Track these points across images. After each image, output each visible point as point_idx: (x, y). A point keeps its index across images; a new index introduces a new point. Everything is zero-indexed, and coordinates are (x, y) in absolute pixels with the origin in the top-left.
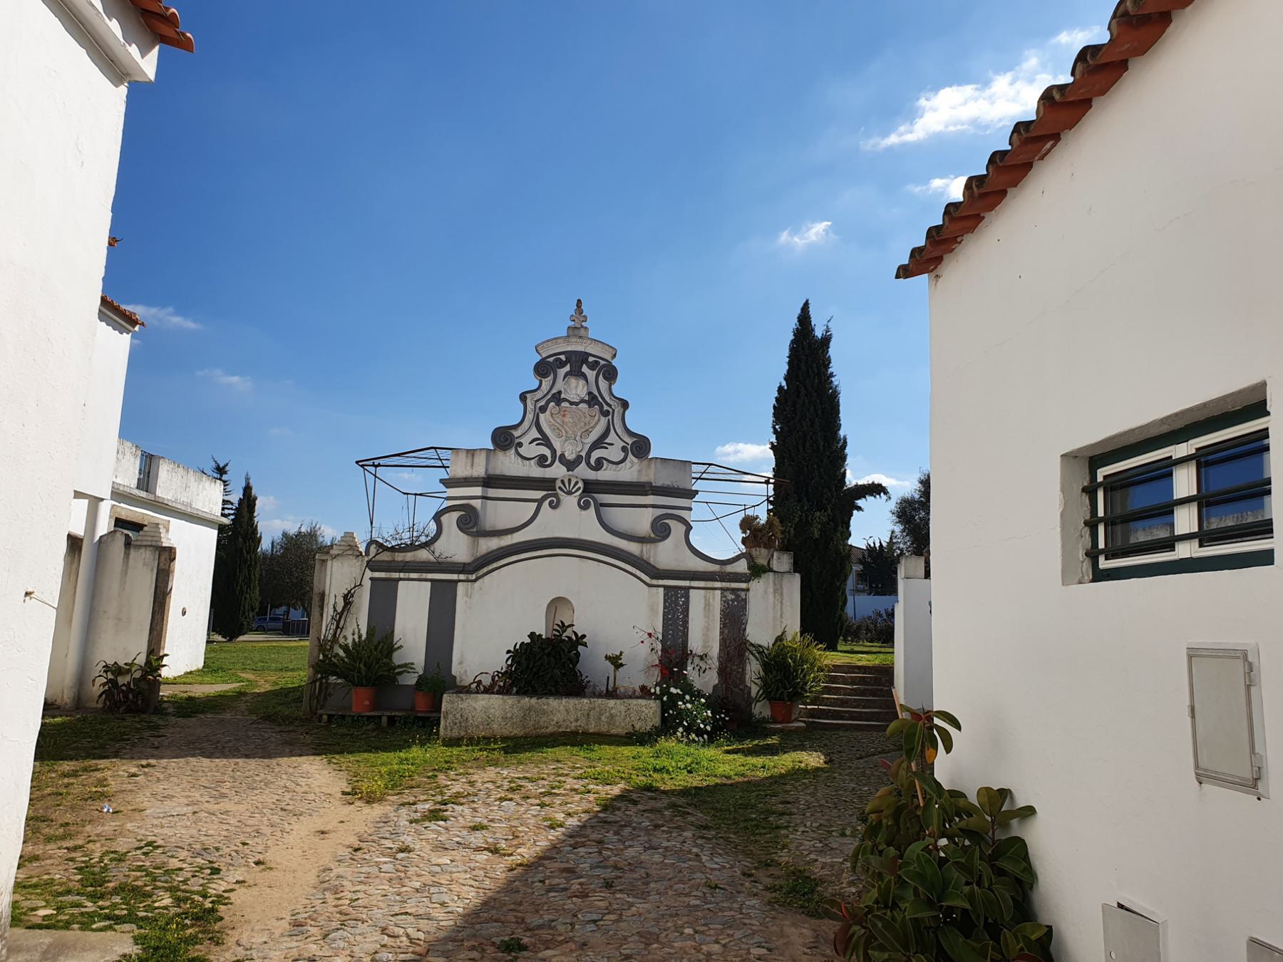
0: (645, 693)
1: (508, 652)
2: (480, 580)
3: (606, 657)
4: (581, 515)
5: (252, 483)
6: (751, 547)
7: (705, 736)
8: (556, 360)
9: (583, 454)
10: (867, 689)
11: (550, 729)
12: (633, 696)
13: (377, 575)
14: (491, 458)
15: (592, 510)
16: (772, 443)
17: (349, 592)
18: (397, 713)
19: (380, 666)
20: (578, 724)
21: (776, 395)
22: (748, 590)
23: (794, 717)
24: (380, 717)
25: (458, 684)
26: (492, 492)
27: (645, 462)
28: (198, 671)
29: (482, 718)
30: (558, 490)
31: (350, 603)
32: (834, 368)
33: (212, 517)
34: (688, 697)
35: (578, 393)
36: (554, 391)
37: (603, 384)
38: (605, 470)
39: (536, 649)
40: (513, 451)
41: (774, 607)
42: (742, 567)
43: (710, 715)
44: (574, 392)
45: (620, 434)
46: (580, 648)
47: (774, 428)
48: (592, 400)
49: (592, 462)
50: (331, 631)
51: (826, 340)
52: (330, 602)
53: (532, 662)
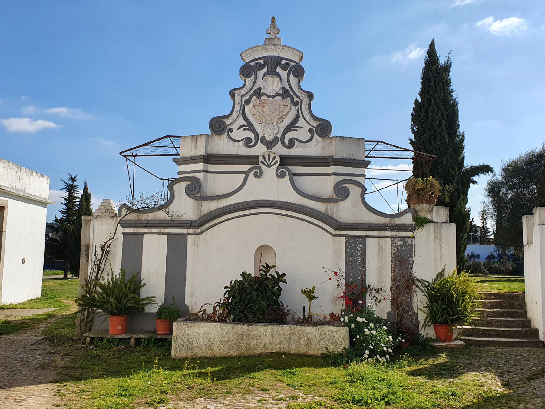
0: (334, 320)
1: (226, 287)
2: (204, 233)
3: (302, 291)
4: (278, 182)
5: (88, 186)
6: (415, 204)
7: (388, 357)
8: (257, 63)
9: (279, 136)
10: (506, 312)
11: (259, 351)
12: (324, 323)
13: (127, 230)
14: (210, 142)
15: (287, 178)
16: (411, 140)
17: (106, 243)
18: (142, 336)
19: (128, 300)
20: (282, 346)
21: (414, 106)
22: (414, 237)
23: (454, 336)
24: (130, 339)
25: (190, 311)
26: (211, 167)
27: (328, 141)
28: (38, 299)
29: (204, 342)
30: (260, 163)
31: (108, 252)
32: (453, 86)
33: (40, 199)
34: (372, 325)
35: (274, 88)
36: (256, 88)
37: (293, 80)
38: (297, 147)
39: (246, 285)
40: (226, 135)
41: (435, 250)
42: (408, 219)
43: (391, 339)
44: (271, 88)
45: (307, 119)
46: (281, 284)
47: (412, 129)
48: (285, 93)
49: (286, 141)
50: (94, 274)
51: (447, 68)
52: (92, 251)
53: (244, 295)
